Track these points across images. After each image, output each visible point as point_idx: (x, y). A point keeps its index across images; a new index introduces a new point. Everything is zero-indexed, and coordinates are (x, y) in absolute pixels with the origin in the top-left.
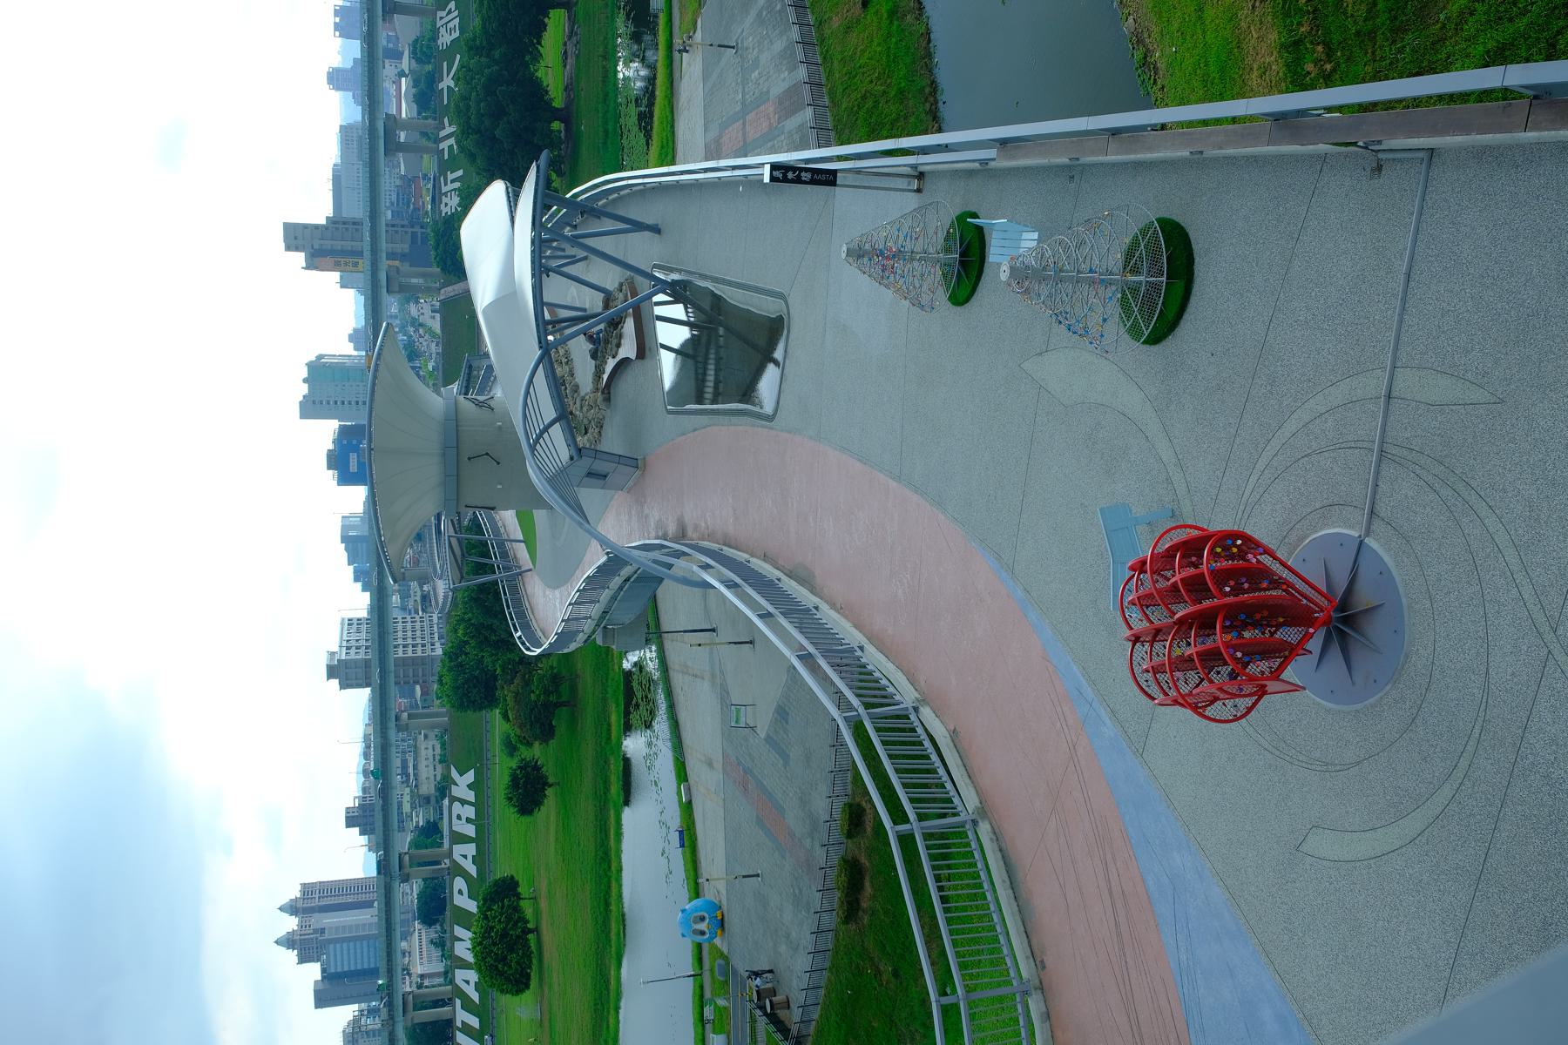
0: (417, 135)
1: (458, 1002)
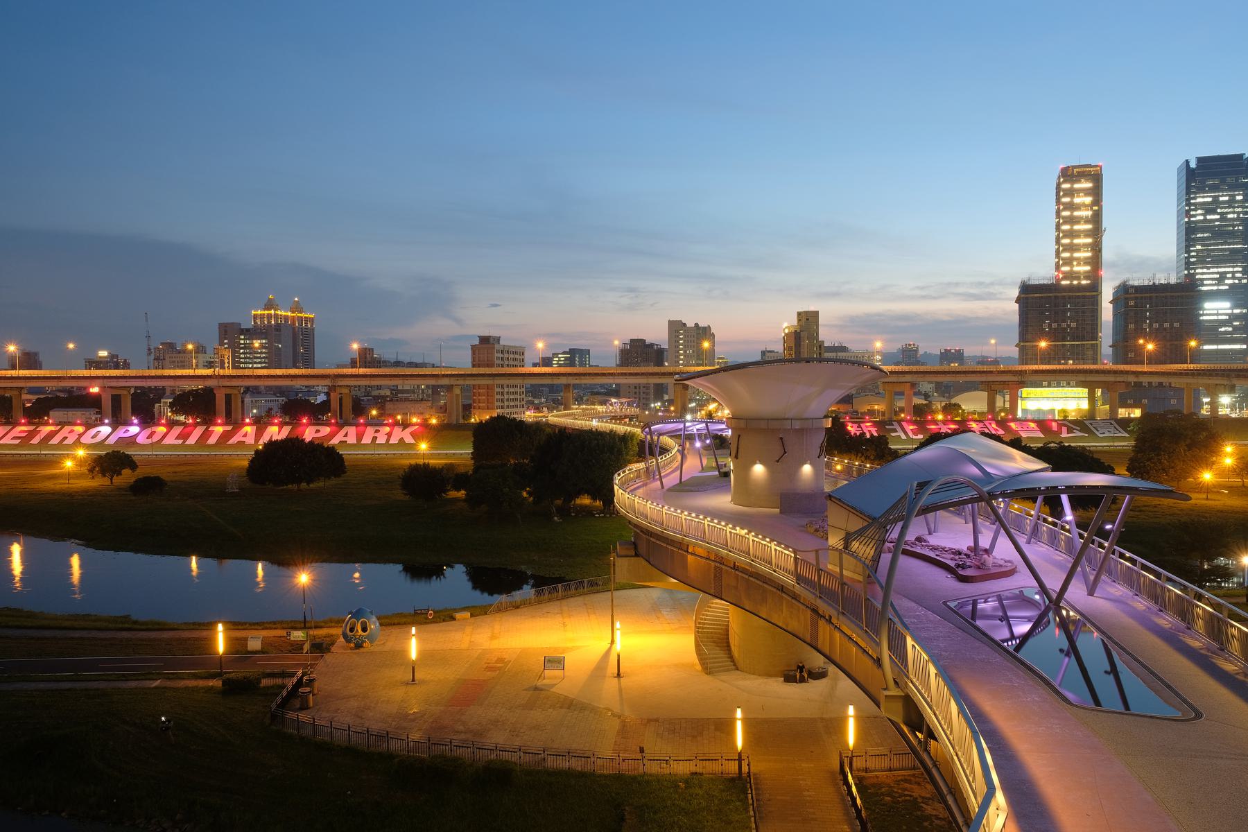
0: (156, 431)
1: (230, 428)
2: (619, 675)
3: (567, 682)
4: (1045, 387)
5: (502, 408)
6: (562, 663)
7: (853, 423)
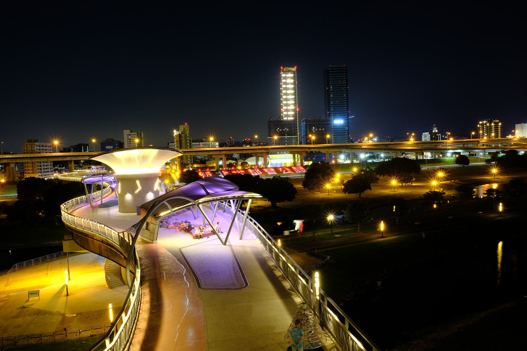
2: (67, 295)
3: (35, 303)
4: (278, 154)
5: (41, 172)
6: (38, 293)
7: (202, 172)
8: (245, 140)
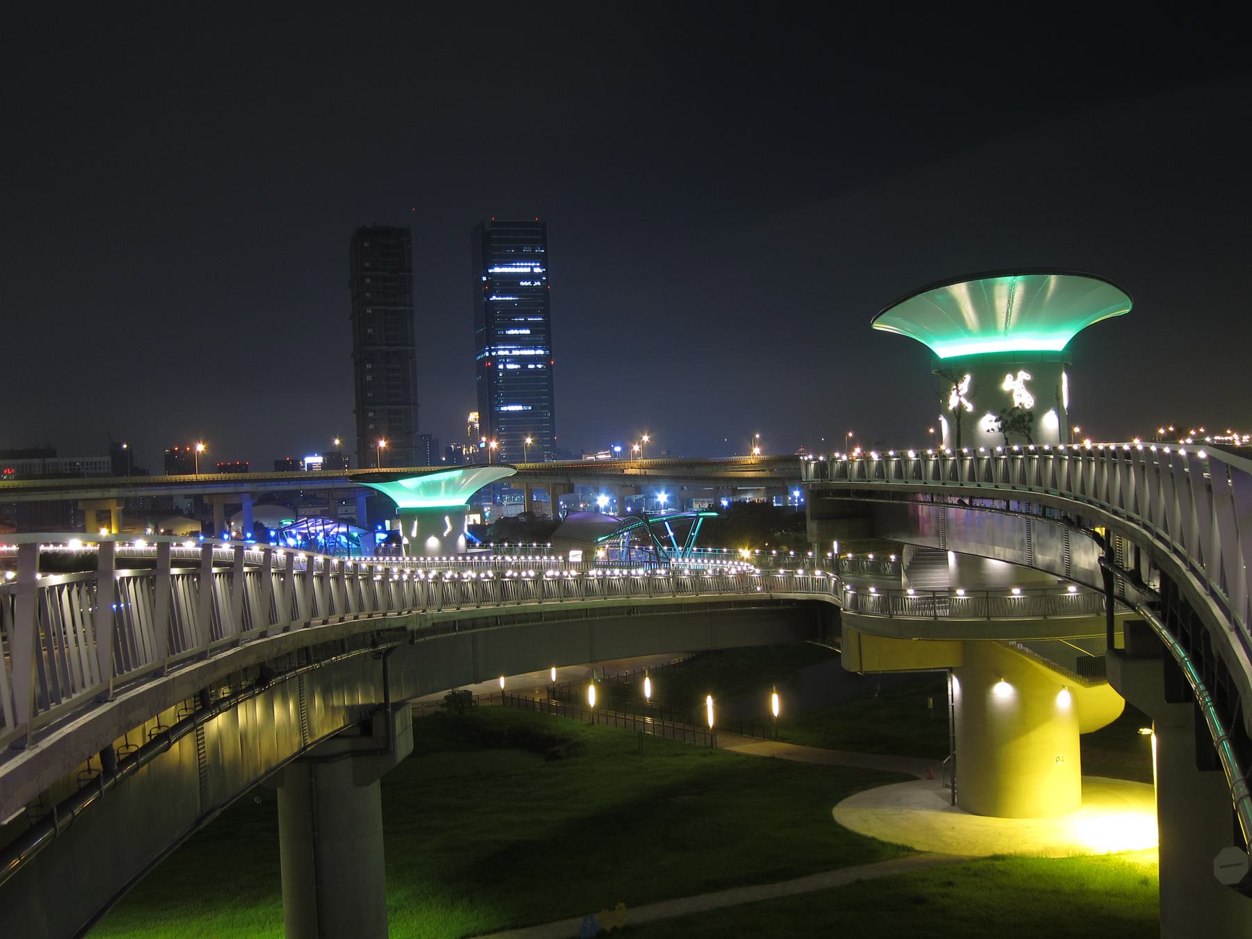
8: (173, 451)
